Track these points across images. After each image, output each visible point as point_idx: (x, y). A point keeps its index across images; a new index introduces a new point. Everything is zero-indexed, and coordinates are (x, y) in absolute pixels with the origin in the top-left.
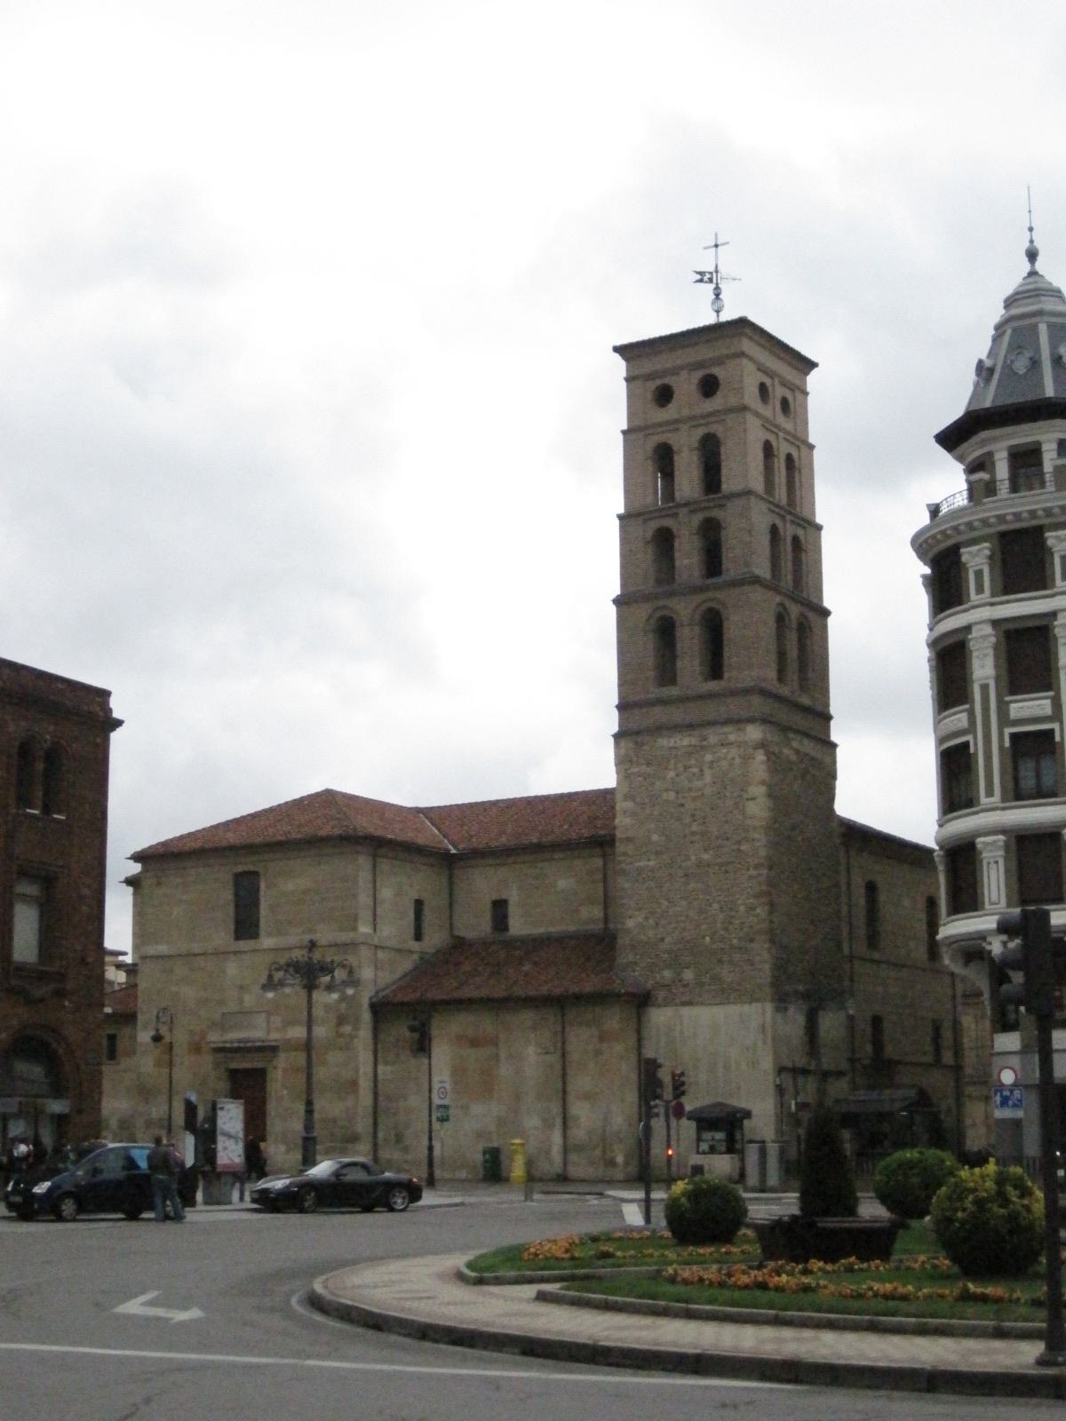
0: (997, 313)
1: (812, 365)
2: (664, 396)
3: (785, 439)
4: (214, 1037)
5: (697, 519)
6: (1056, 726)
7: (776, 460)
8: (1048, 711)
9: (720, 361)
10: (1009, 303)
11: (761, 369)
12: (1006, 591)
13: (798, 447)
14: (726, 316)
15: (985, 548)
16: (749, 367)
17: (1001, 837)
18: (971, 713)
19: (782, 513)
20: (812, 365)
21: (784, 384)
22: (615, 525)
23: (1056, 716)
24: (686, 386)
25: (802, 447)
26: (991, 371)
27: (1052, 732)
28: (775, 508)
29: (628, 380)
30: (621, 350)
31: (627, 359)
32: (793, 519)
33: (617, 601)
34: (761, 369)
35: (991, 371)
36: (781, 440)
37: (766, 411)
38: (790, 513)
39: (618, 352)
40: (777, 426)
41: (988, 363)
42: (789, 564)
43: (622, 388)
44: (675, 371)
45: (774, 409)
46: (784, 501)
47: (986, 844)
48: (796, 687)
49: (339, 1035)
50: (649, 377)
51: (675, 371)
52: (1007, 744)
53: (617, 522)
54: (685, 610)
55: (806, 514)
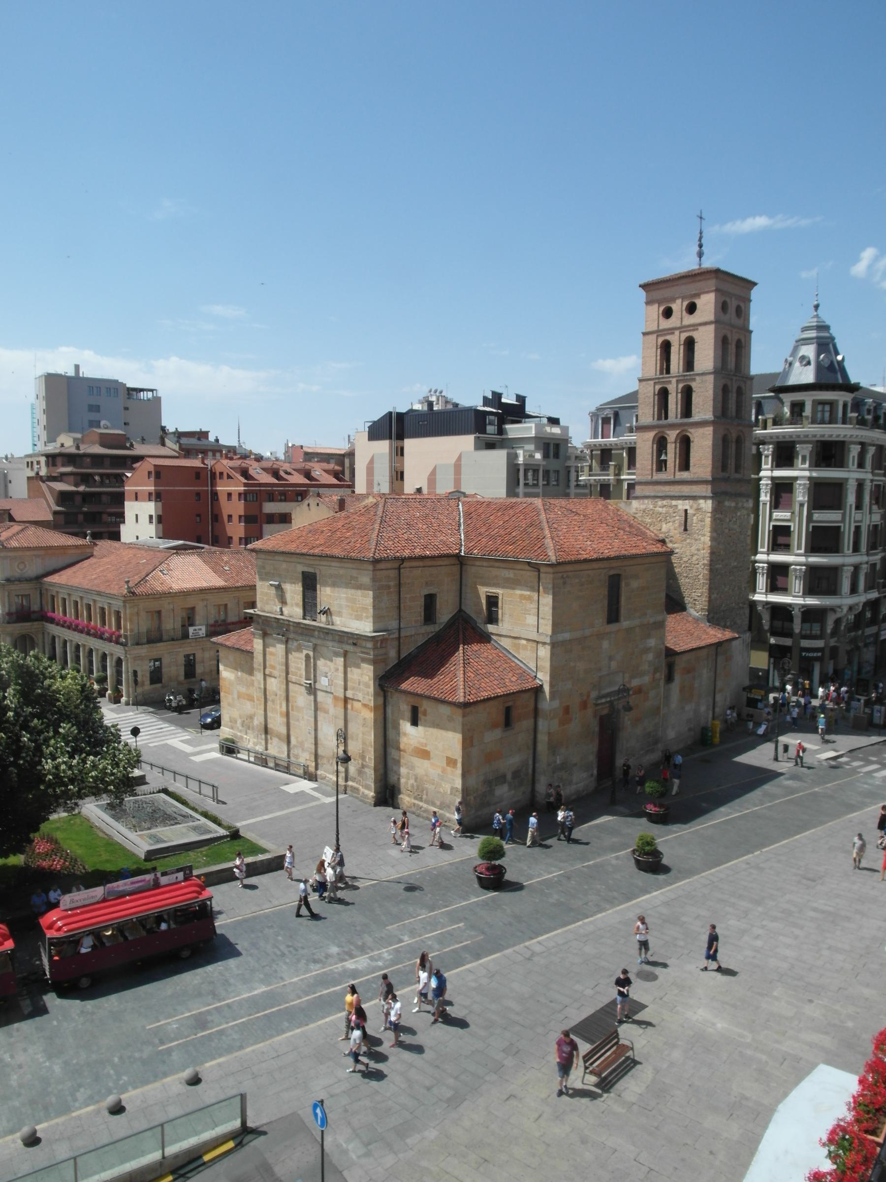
6: (842, 525)
8: (840, 519)
12: (816, 466)
15: (810, 447)
17: (766, 565)
18: (844, 515)
23: (843, 520)
27: (789, 527)
30: (644, 286)
31: (646, 292)
44: (673, 300)
52: (811, 530)
54: (672, 436)
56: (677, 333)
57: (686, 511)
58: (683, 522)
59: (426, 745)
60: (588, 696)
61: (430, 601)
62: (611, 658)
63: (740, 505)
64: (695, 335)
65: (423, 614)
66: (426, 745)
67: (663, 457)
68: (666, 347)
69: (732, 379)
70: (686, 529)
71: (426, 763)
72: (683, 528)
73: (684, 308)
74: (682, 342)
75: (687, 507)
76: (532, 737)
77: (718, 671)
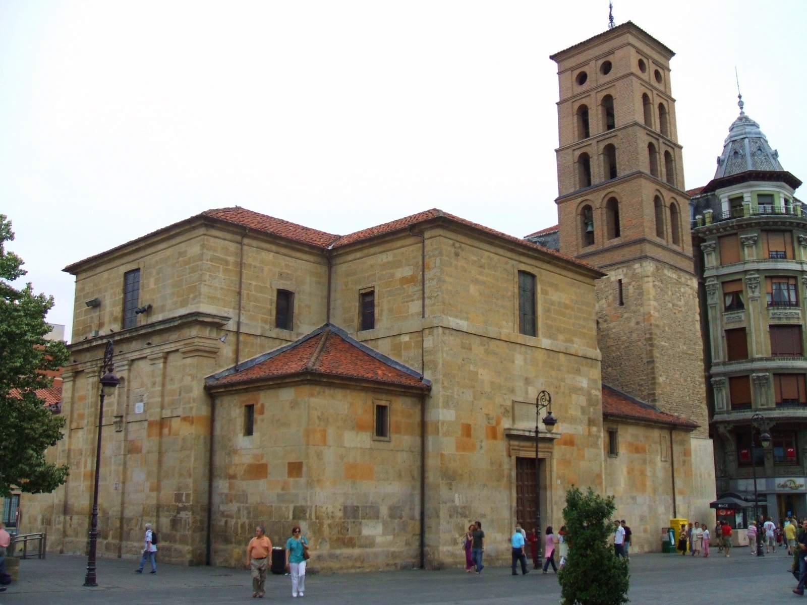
0: (726, 134)
1: (672, 54)
2: (582, 78)
4: (506, 424)
5: (602, 146)
9: (611, 52)
10: (731, 129)
11: (639, 51)
13: (667, 101)
14: (618, 22)
16: (633, 51)
19: (657, 137)
20: (672, 54)
21: (655, 62)
22: (555, 108)
26: (723, 161)
28: (650, 133)
29: (559, 73)
31: (558, 62)
32: (664, 141)
33: (557, 201)
34: (639, 51)
35: (723, 161)
36: (655, 95)
37: (645, 76)
38: (662, 137)
39: (553, 59)
40: (652, 86)
41: (722, 158)
42: (664, 170)
43: (556, 78)
44: (586, 63)
45: (649, 75)
46: (658, 130)
47: (716, 381)
48: (670, 240)
49: (590, 434)
50: (572, 69)
51: (586, 63)
53: (556, 106)
54: (597, 200)
55: (673, 140)
56: (593, 94)
57: (620, 281)
58: (618, 295)
59: (262, 456)
60: (498, 423)
61: (285, 298)
62: (527, 381)
63: (683, 280)
64: (612, 92)
65: (274, 312)
66: (262, 456)
67: (590, 229)
68: (583, 112)
69: (658, 140)
70: (622, 304)
71: (262, 484)
72: (618, 302)
73: (598, 69)
74: (600, 102)
75: (621, 277)
76: (419, 463)
77: (675, 466)
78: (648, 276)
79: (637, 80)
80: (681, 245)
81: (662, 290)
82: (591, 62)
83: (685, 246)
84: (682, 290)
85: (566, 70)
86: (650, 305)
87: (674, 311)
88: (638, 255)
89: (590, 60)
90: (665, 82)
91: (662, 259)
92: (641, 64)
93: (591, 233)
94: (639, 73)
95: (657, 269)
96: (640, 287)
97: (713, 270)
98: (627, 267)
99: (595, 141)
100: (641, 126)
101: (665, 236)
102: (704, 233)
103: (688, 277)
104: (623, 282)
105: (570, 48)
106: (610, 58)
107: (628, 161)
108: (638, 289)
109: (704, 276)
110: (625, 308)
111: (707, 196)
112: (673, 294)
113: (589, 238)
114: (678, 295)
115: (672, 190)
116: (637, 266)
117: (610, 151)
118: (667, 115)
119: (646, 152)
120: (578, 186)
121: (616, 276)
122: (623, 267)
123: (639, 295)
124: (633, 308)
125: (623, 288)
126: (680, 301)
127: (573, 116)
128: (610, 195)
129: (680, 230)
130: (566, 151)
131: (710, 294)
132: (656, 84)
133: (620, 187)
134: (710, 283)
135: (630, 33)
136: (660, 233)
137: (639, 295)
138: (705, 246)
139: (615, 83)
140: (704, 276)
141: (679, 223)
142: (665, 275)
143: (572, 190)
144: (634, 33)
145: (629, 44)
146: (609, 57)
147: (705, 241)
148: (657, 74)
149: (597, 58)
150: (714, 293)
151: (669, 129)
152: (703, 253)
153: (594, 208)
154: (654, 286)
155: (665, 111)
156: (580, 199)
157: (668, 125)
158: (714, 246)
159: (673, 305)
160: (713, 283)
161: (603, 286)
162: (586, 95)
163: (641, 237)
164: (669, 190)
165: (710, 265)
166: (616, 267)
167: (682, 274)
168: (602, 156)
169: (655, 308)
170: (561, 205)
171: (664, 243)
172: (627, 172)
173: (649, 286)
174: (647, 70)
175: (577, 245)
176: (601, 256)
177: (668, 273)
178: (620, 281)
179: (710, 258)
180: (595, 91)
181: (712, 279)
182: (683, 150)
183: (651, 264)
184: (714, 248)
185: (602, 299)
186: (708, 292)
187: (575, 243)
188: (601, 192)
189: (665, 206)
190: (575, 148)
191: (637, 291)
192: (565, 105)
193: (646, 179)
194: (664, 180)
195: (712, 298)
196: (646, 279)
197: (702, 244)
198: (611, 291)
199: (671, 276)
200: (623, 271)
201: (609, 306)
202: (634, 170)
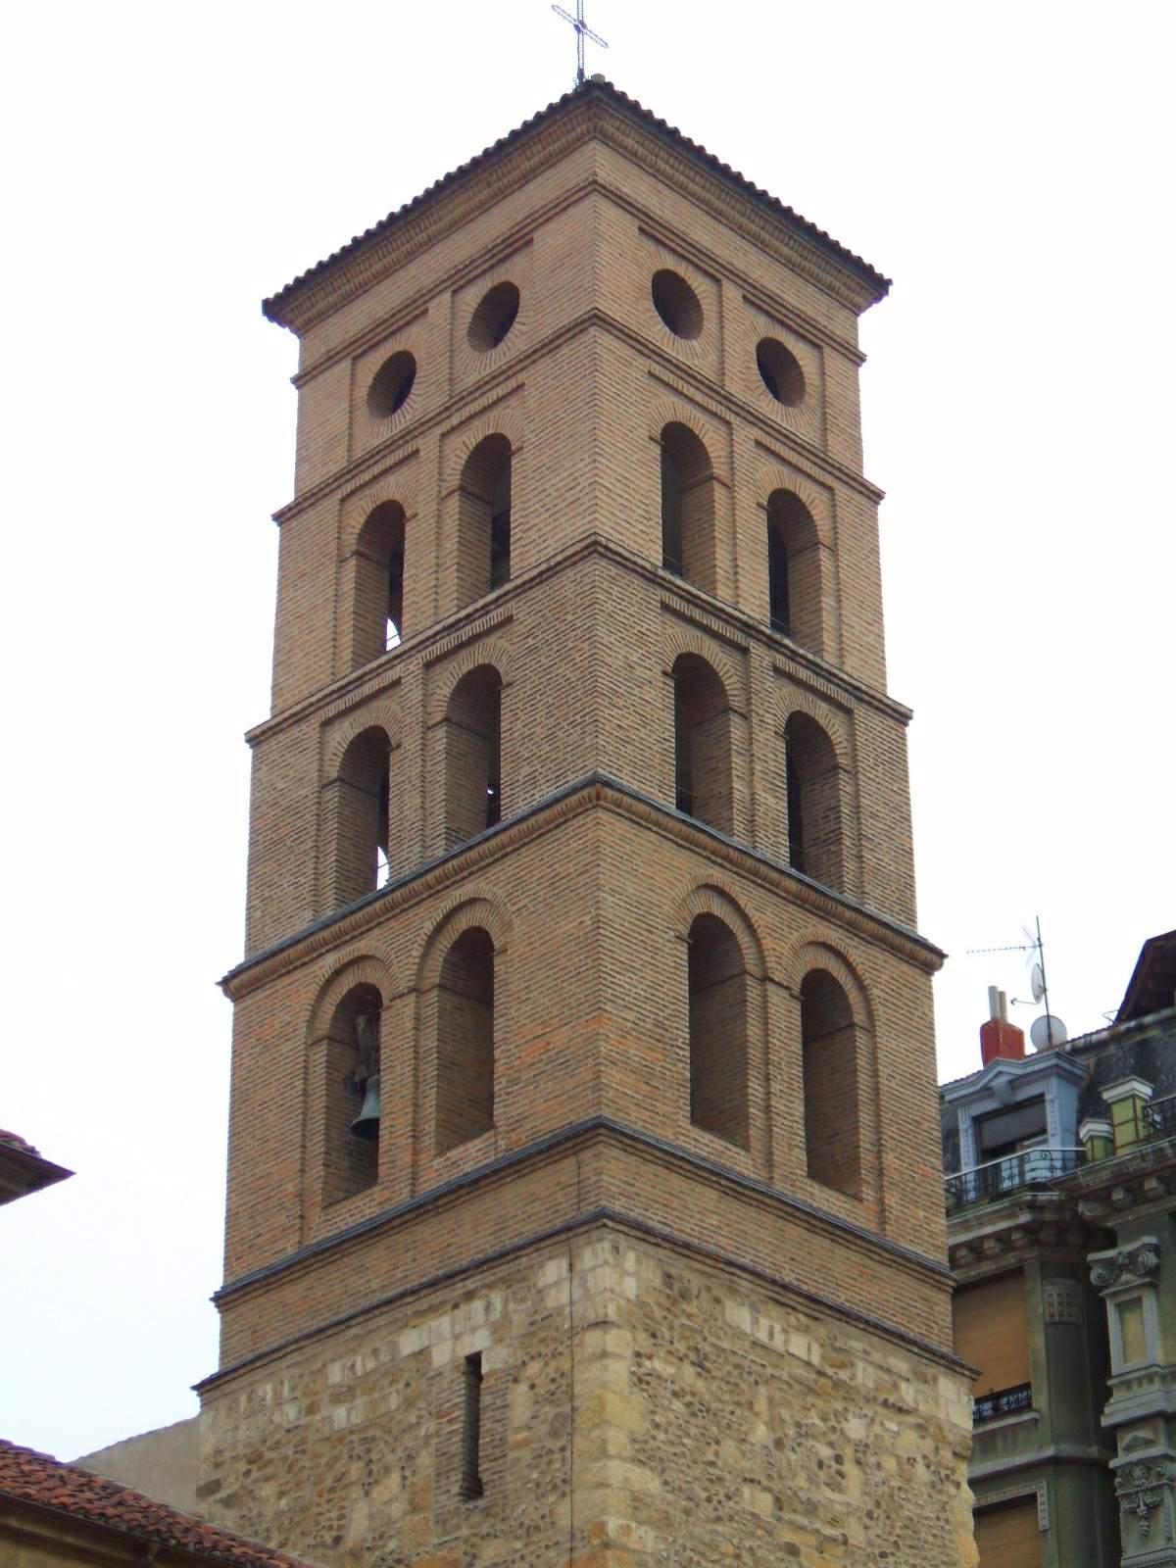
1: (875, 286)
2: (395, 383)
3: (778, 671)
7: (736, 729)
9: (517, 242)
11: (652, 230)
19: (738, 637)
20: (875, 286)
24: (438, 340)
25: (861, 712)
32: (782, 661)
36: (744, 448)
39: (282, 322)
40: (727, 400)
44: (413, 311)
48: (792, 1155)
50: (357, 349)
54: (402, 956)
55: (853, 668)
57: (474, 1361)
58: (456, 1446)
67: (368, 1111)
72: (455, 1483)
75: (479, 1341)
78: (603, 1324)
79: (627, 353)
80: (868, 1193)
81: (697, 1408)
82: (431, 305)
83: (892, 1199)
84: (855, 1428)
85: (330, 360)
86: (604, 1485)
87: (787, 1536)
88: (567, 1213)
89: (432, 293)
90: (824, 402)
91: (721, 1242)
92: (673, 302)
93: (369, 1130)
94: (656, 331)
95: (675, 1293)
96: (561, 1393)
97: (1146, 1387)
98: (507, 1282)
99: (415, 663)
100: (624, 562)
101: (755, 1132)
102: (1102, 1196)
103: (900, 1363)
104: (485, 1369)
105: (346, 251)
106: (513, 271)
107: (550, 737)
108: (551, 1398)
109: (1105, 1422)
110: (487, 1512)
111: (1141, 1028)
112: (779, 1444)
113: (361, 1142)
114: (825, 1452)
115: (822, 908)
116: (553, 1271)
117: (481, 699)
118: (824, 555)
119: (659, 701)
120: (330, 896)
121: (457, 1337)
122: (490, 1286)
123: (554, 1434)
124: (526, 1509)
125: (486, 1399)
126: (836, 1487)
127: (342, 561)
128: (462, 923)
129: (865, 1117)
130: (295, 732)
131: (1133, 1512)
132: (766, 405)
133: (508, 868)
134: (1135, 1456)
135: (607, 139)
136: (715, 1103)
137: (554, 1434)
138: (1109, 1263)
139: (521, 378)
140: (1105, 1422)
141: (863, 1079)
142: (737, 1334)
143: (303, 922)
144: (629, 142)
145: (594, 187)
146: (507, 265)
147: (1110, 1240)
148: (777, 370)
149: (457, 282)
150: (1153, 1508)
151: (828, 620)
152: (1102, 1303)
153: (385, 997)
154: (640, 1381)
155: (811, 540)
156: (330, 961)
157: (827, 601)
158: (1151, 1259)
159: (779, 1502)
160: (1153, 1452)
161: (394, 1402)
162: (399, 454)
163: (585, 1116)
164: (798, 901)
165: (1136, 1362)
166: (460, 1288)
167: (857, 1342)
168: (441, 732)
169: (637, 1501)
170: (249, 1001)
171: (743, 1164)
172: (546, 792)
173: (609, 1374)
174: (710, 324)
175: (300, 1195)
176: (401, 1239)
177: (747, 1319)
178: (474, 1361)
179: (1132, 1318)
180: (439, 431)
181: (1143, 1433)
182: (912, 730)
183: (630, 1260)
184: (1154, 1272)
185: (387, 1470)
186: (1124, 1505)
187: (290, 1188)
188: (421, 909)
189: (766, 979)
190: (332, 710)
191: (549, 1411)
192: (311, 517)
193: (638, 821)
194: (775, 848)
195: (1145, 1536)
196: (593, 1339)
197: (1092, 1257)
198: (431, 1426)
199: (778, 1342)
200: (488, 1308)
201: (415, 1508)
202: (574, 779)
